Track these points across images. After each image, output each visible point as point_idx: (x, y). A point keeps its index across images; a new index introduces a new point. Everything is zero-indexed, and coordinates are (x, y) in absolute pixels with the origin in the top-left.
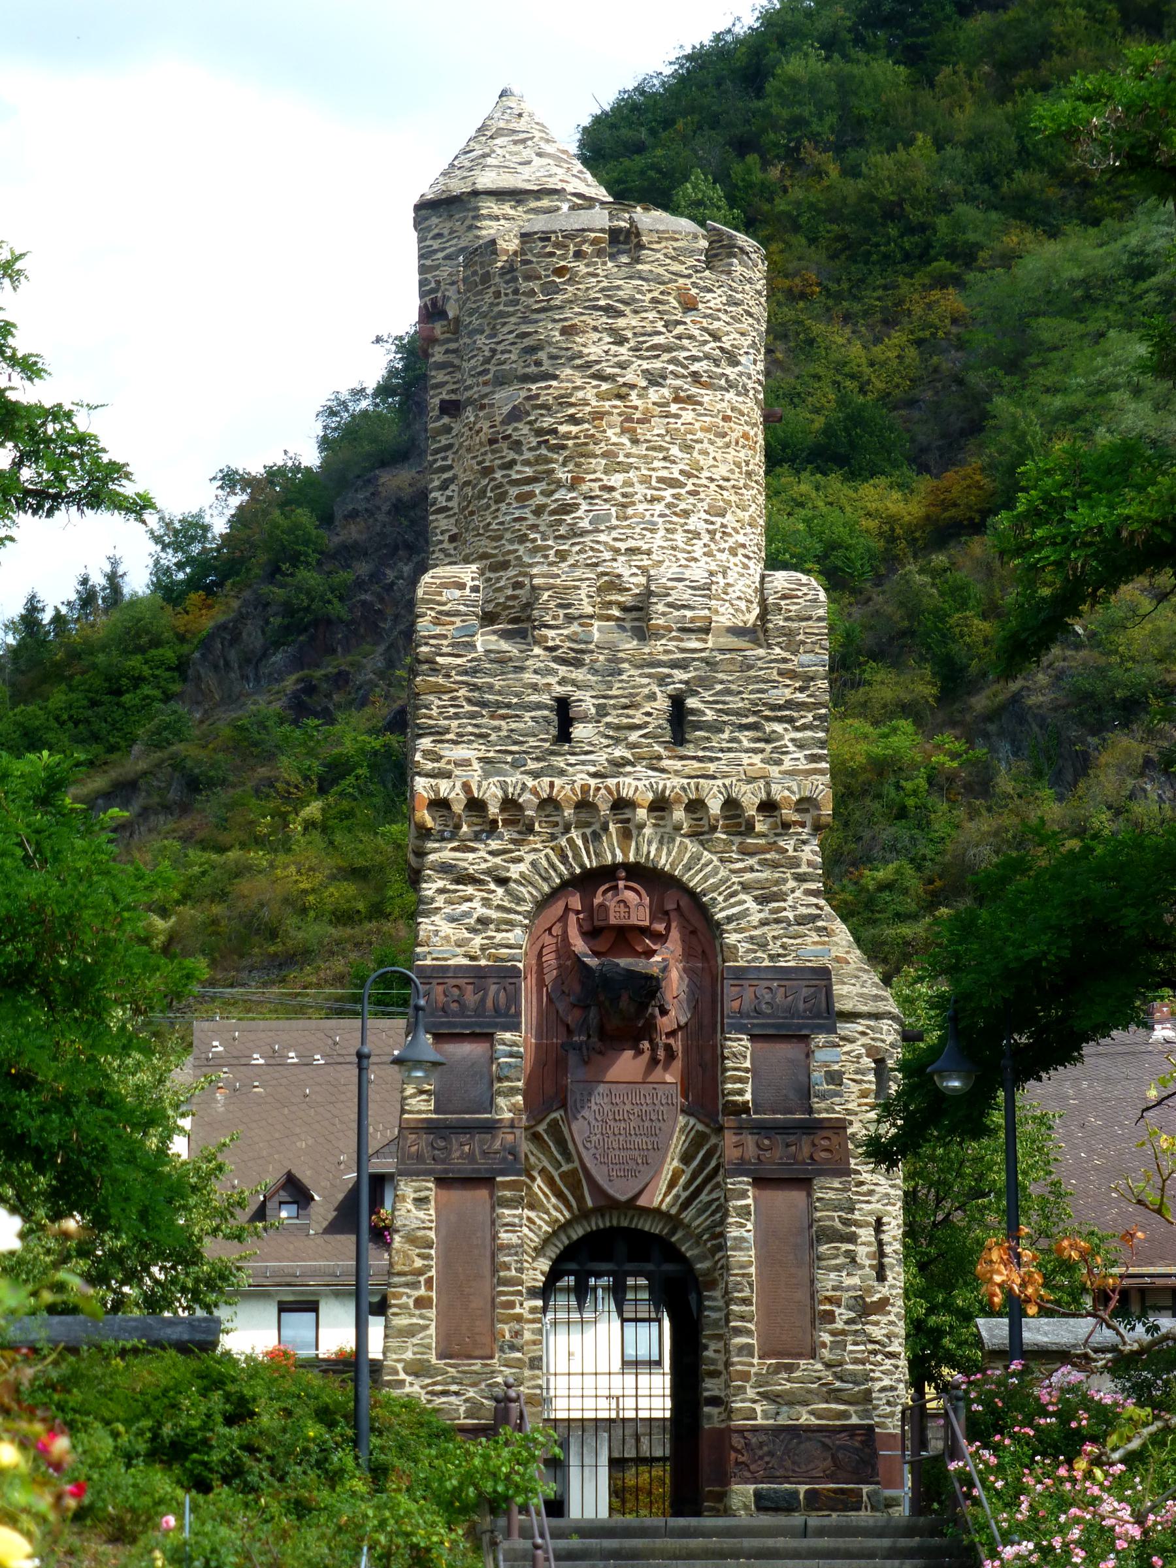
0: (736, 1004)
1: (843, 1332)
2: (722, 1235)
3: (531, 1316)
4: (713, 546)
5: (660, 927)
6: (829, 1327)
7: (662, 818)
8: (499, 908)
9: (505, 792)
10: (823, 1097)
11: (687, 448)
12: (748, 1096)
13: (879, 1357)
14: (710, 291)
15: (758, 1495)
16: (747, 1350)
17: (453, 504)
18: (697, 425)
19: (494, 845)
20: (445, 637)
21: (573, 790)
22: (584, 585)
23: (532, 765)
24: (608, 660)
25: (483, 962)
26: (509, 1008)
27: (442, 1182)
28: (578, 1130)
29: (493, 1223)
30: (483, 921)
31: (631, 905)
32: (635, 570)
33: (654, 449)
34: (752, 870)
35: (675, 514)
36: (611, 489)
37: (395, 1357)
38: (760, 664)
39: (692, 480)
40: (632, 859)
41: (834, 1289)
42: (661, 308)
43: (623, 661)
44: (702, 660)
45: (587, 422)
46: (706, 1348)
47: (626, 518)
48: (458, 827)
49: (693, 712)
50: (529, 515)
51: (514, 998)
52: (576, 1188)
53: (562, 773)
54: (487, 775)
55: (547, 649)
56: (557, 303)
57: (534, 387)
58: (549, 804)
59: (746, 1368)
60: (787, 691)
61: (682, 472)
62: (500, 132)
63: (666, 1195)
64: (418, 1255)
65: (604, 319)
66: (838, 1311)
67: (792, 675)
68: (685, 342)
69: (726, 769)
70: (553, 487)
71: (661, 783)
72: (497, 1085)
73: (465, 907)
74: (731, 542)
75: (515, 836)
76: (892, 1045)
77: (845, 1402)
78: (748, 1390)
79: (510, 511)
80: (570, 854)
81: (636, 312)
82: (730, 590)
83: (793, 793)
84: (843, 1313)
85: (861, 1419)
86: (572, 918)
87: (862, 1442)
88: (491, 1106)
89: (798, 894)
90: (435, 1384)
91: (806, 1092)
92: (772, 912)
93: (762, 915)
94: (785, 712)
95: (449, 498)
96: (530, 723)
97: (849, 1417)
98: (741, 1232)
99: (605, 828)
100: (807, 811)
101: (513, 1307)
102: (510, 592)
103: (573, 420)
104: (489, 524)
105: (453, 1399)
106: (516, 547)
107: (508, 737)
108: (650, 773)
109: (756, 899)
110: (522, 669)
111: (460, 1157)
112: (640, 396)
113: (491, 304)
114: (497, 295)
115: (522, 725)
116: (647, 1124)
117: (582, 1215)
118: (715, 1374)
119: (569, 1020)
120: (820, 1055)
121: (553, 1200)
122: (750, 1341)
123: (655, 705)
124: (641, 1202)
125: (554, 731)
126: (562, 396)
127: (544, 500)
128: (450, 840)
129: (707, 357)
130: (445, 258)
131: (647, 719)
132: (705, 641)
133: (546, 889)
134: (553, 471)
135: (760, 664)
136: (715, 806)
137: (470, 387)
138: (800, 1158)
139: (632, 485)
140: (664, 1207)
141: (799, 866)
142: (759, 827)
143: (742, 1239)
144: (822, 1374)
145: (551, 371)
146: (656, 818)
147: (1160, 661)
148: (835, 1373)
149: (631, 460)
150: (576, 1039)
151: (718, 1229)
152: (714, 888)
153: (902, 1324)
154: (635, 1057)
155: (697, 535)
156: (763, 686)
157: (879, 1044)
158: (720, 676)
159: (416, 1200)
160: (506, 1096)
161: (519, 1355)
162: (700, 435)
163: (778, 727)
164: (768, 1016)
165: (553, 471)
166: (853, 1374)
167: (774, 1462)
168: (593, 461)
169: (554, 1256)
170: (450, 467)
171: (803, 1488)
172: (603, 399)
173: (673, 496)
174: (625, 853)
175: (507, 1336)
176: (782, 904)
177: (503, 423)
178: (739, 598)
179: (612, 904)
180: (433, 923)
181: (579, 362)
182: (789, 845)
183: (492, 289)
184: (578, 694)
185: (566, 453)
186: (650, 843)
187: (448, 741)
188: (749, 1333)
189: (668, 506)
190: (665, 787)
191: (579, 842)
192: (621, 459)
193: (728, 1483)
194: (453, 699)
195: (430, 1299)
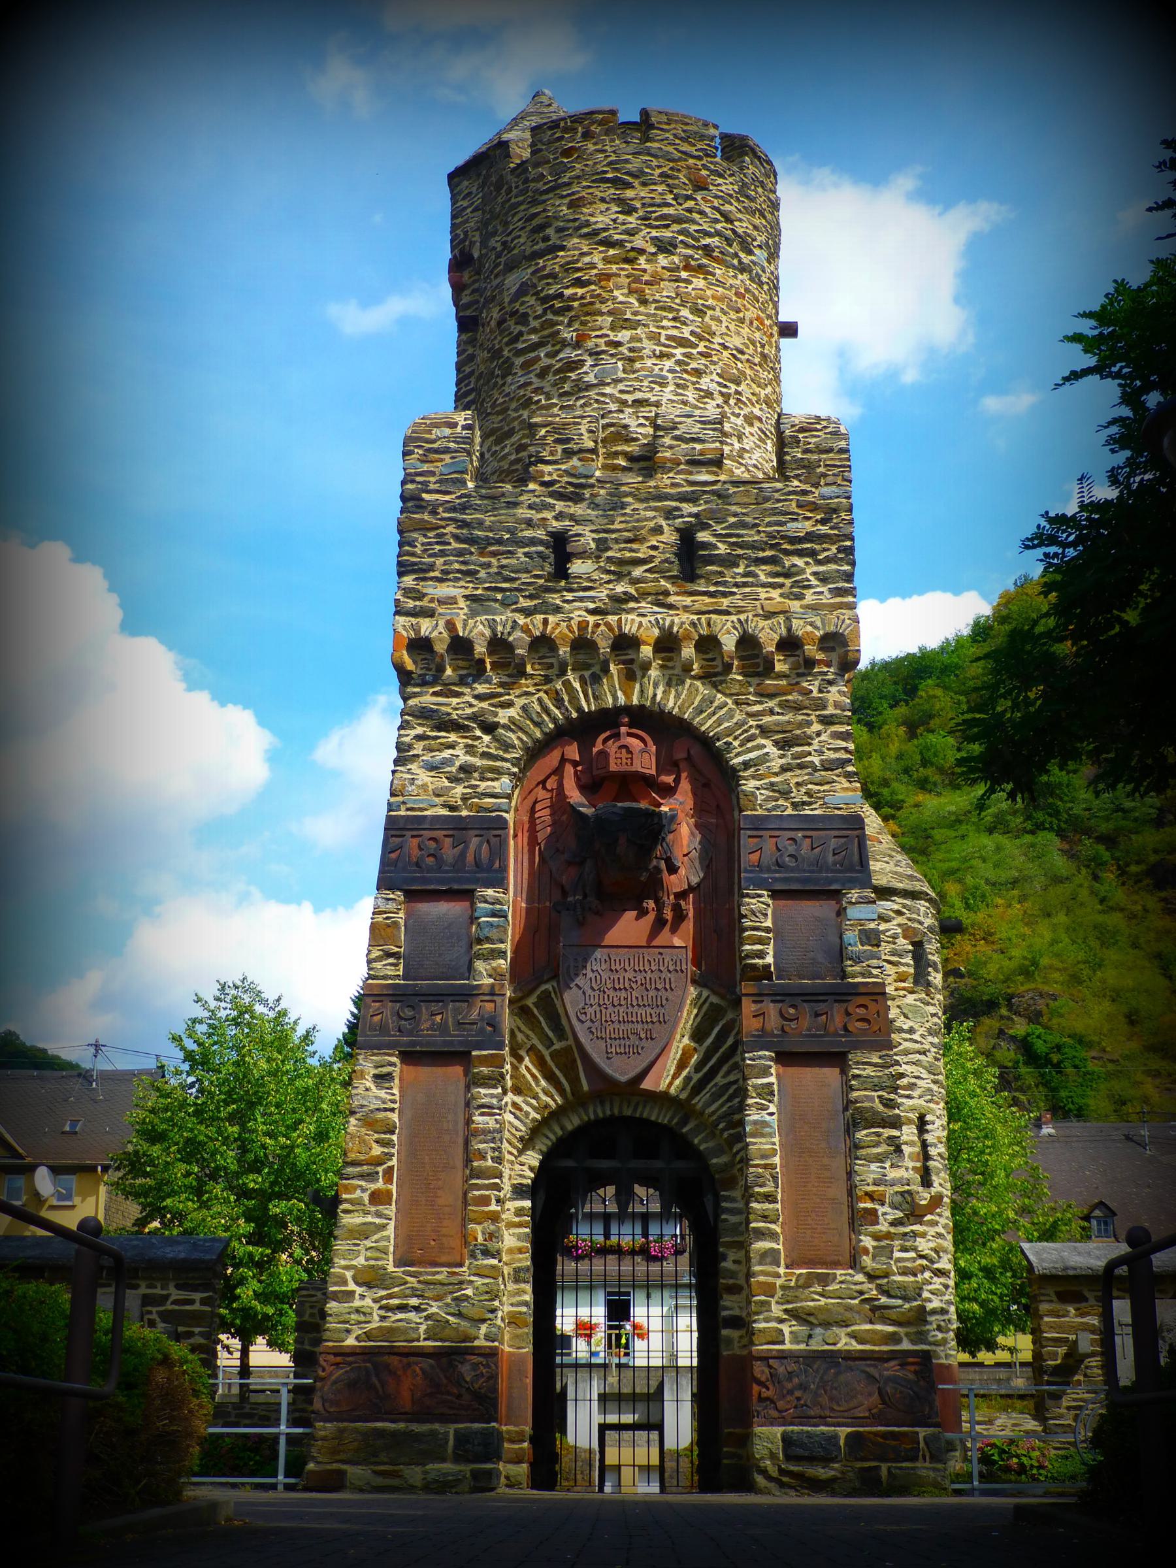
0: (755, 857)
1: (888, 1236)
2: (741, 1123)
3: (517, 1219)
4: (726, 408)
5: (669, 779)
6: (871, 1229)
7: (670, 659)
8: (485, 755)
10: (857, 960)
11: (699, 311)
12: (769, 959)
13: (927, 1275)
14: (721, 176)
15: (787, 1439)
16: (771, 1257)
18: (709, 293)
19: (481, 688)
20: (433, 473)
24: (610, 494)
25: (464, 813)
26: (492, 862)
27: (409, 1057)
28: (571, 1000)
29: (467, 1104)
30: (466, 769)
31: (638, 754)
33: (663, 308)
34: (772, 712)
35: (686, 371)
36: (618, 344)
37: (343, 1263)
38: (777, 495)
39: (702, 344)
40: (635, 702)
41: (876, 1183)
42: (670, 181)
44: (713, 492)
46: (724, 1257)
47: (634, 372)
48: (441, 669)
49: (705, 545)
50: (534, 380)
51: (499, 851)
52: (569, 1069)
53: (557, 610)
54: (473, 614)
55: (544, 484)
56: (565, 180)
58: (542, 644)
59: (771, 1279)
60: (808, 524)
61: (692, 333)
63: (674, 1077)
64: (377, 1142)
65: (612, 191)
67: (814, 507)
68: (696, 216)
69: (741, 603)
70: (558, 347)
71: (668, 619)
73: (446, 754)
74: (746, 411)
75: (505, 679)
76: (930, 929)
77: (894, 1323)
78: (774, 1307)
80: (566, 698)
81: (644, 184)
82: (746, 455)
83: (816, 628)
84: (887, 1213)
85: (913, 1342)
86: (569, 770)
87: (916, 1372)
89: (823, 737)
90: (390, 1296)
91: (840, 953)
92: (794, 757)
93: (784, 761)
96: (523, 559)
99: (606, 671)
100: (833, 649)
102: (513, 457)
103: (579, 283)
105: (412, 1315)
107: (498, 573)
108: (656, 609)
109: (776, 743)
110: (515, 505)
116: (652, 993)
117: (575, 1101)
118: (735, 1290)
119: (564, 879)
120: (853, 913)
121: (543, 1083)
122: (774, 1246)
123: (662, 538)
124: (647, 1085)
125: (549, 568)
126: (568, 263)
129: (718, 233)
135: (777, 495)
136: (729, 642)
138: (832, 1029)
139: (640, 340)
140: (672, 1090)
141: (825, 707)
142: (779, 667)
143: (765, 1124)
145: (558, 243)
146: (663, 659)
147: (1004, 982)
148: (879, 1287)
151: (737, 1117)
152: (729, 732)
153: (950, 1237)
154: (637, 918)
155: (709, 394)
156: (781, 518)
157: (916, 925)
159: (377, 1077)
161: (494, 1262)
162: (710, 302)
163: (800, 562)
164: (792, 870)
165: (558, 332)
166: (902, 1287)
167: (807, 1398)
168: (600, 318)
169: (544, 1149)
171: (843, 1431)
172: (610, 263)
173: (684, 354)
174: (628, 696)
175: (480, 1238)
176: (806, 748)
178: (755, 466)
180: (409, 771)
181: (586, 230)
184: (577, 529)
186: (656, 685)
187: (431, 579)
188: (773, 1236)
189: (678, 362)
190: (673, 622)
191: (577, 685)
192: (628, 316)
193: (750, 1425)
195: (389, 1193)
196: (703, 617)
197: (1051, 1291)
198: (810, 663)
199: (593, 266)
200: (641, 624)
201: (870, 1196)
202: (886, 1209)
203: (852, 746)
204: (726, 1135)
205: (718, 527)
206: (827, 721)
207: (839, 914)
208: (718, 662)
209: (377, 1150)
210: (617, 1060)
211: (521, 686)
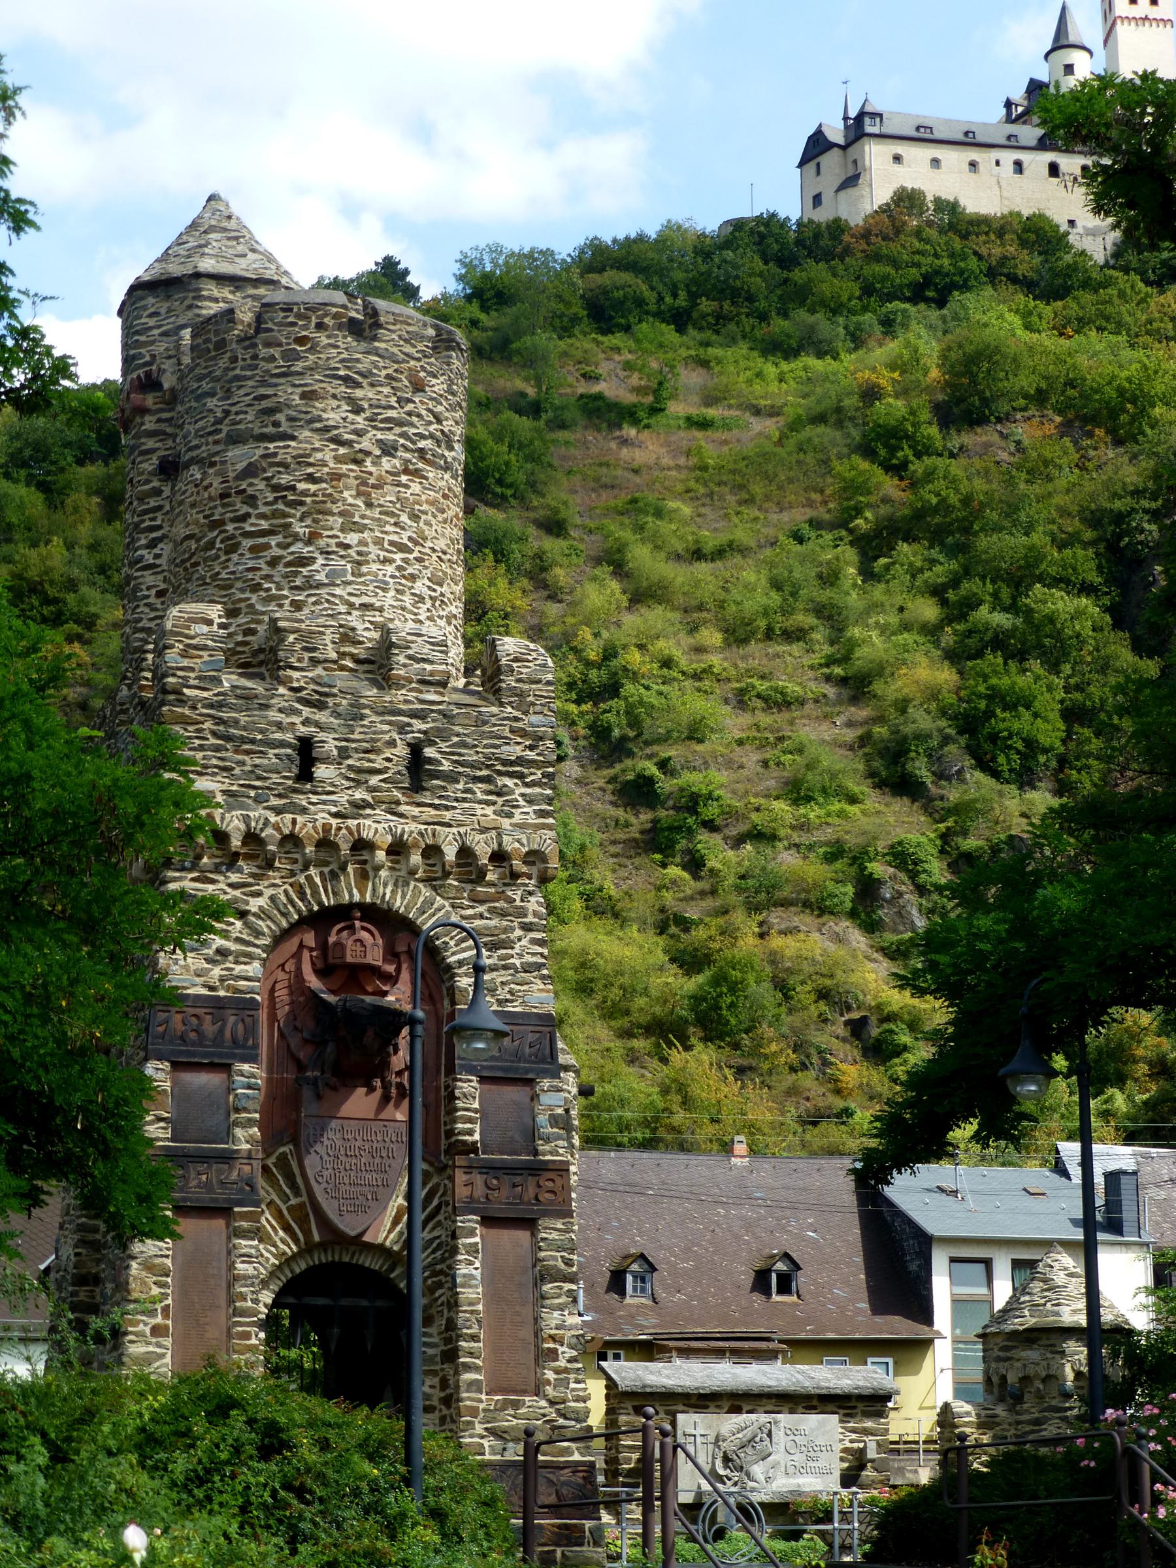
1: (566, 1370)
5: (391, 968)
6: (553, 1364)
7: (397, 862)
9: (248, 826)
10: (547, 1140)
11: (415, 517)
12: (477, 1137)
14: (435, 376)
16: (474, 1385)
17: (162, 561)
18: (424, 498)
19: (234, 878)
20: (192, 669)
21: (314, 828)
22: (328, 631)
23: (275, 802)
24: (351, 705)
25: (222, 993)
26: (246, 1039)
29: (229, 1253)
30: (222, 953)
31: (366, 946)
32: (368, 625)
33: (386, 513)
34: (481, 917)
35: (404, 577)
36: (347, 547)
40: (368, 900)
42: (395, 384)
43: (365, 707)
44: (439, 712)
45: (325, 481)
47: (361, 575)
48: (199, 857)
49: (431, 761)
50: (264, 566)
51: (252, 1030)
52: (303, 1222)
53: (304, 811)
54: (230, 808)
55: (292, 689)
56: (298, 369)
57: (271, 446)
58: (291, 840)
60: (518, 748)
61: (410, 539)
62: (211, 229)
63: (390, 1232)
65: (343, 389)
66: (561, 1349)
67: (524, 733)
68: (415, 419)
70: (289, 540)
72: (234, 1116)
75: (255, 870)
78: (477, 1426)
79: (242, 561)
81: (372, 385)
85: (582, 1455)
86: (306, 955)
88: (228, 1136)
89: (524, 942)
91: (531, 1134)
92: (500, 958)
94: (517, 768)
95: (157, 556)
96: (274, 760)
97: (572, 1454)
98: (470, 1271)
99: (343, 868)
100: (533, 863)
101: (249, 1338)
102: (240, 638)
103: (311, 478)
104: (218, 573)
106: (247, 595)
107: (252, 772)
110: (266, 707)
111: (198, 1186)
112: (374, 463)
113: (227, 369)
114: (234, 359)
115: (266, 762)
116: (377, 1160)
117: (308, 1249)
119: (301, 1055)
120: (546, 1099)
121: (281, 1233)
123: (394, 751)
124: (367, 1238)
125: (296, 770)
126: (301, 456)
127: (280, 552)
128: (190, 870)
129: (432, 436)
130: (161, 335)
131: (387, 764)
132: (442, 694)
133: (285, 924)
134: (290, 524)
136: (450, 853)
137: (197, 447)
140: (388, 1243)
141: (525, 916)
142: (490, 877)
143: (472, 1277)
144: (546, 1411)
145: (289, 431)
148: (558, 1411)
149: (366, 521)
150: (309, 1074)
154: (367, 1094)
155: (421, 599)
158: (456, 728)
160: (243, 1127)
162: (425, 507)
165: (290, 524)
166: (575, 1411)
170: (160, 527)
172: (340, 462)
173: (403, 560)
174: (362, 893)
176: (510, 951)
177: (237, 478)
179: (349, 943)
181: (318, 425)
182: (516, 895)
183: (228, 355)
184: (322, 736)
185: (304, 509)
186: (385, 885)
189: (399, 568)
190: (403, 831)
191: (318, 880)
192: (356, 519)
194: (199, 731)
195: (167, 1327)
196: (430, 827)
197: (629, 1405)
198: (515, 876)
199: (324, 464)
200: (376, 831)
201: (553, 1338)
202: (565, 1349)
203: (546, 952)
204: (429, 1282)
205: (443, 745)
206: (527, 928)
207: (532, 1099)
208: (438, 868)
209: (156, 1291)
210: (347, 1217)
211: (269, 878)
